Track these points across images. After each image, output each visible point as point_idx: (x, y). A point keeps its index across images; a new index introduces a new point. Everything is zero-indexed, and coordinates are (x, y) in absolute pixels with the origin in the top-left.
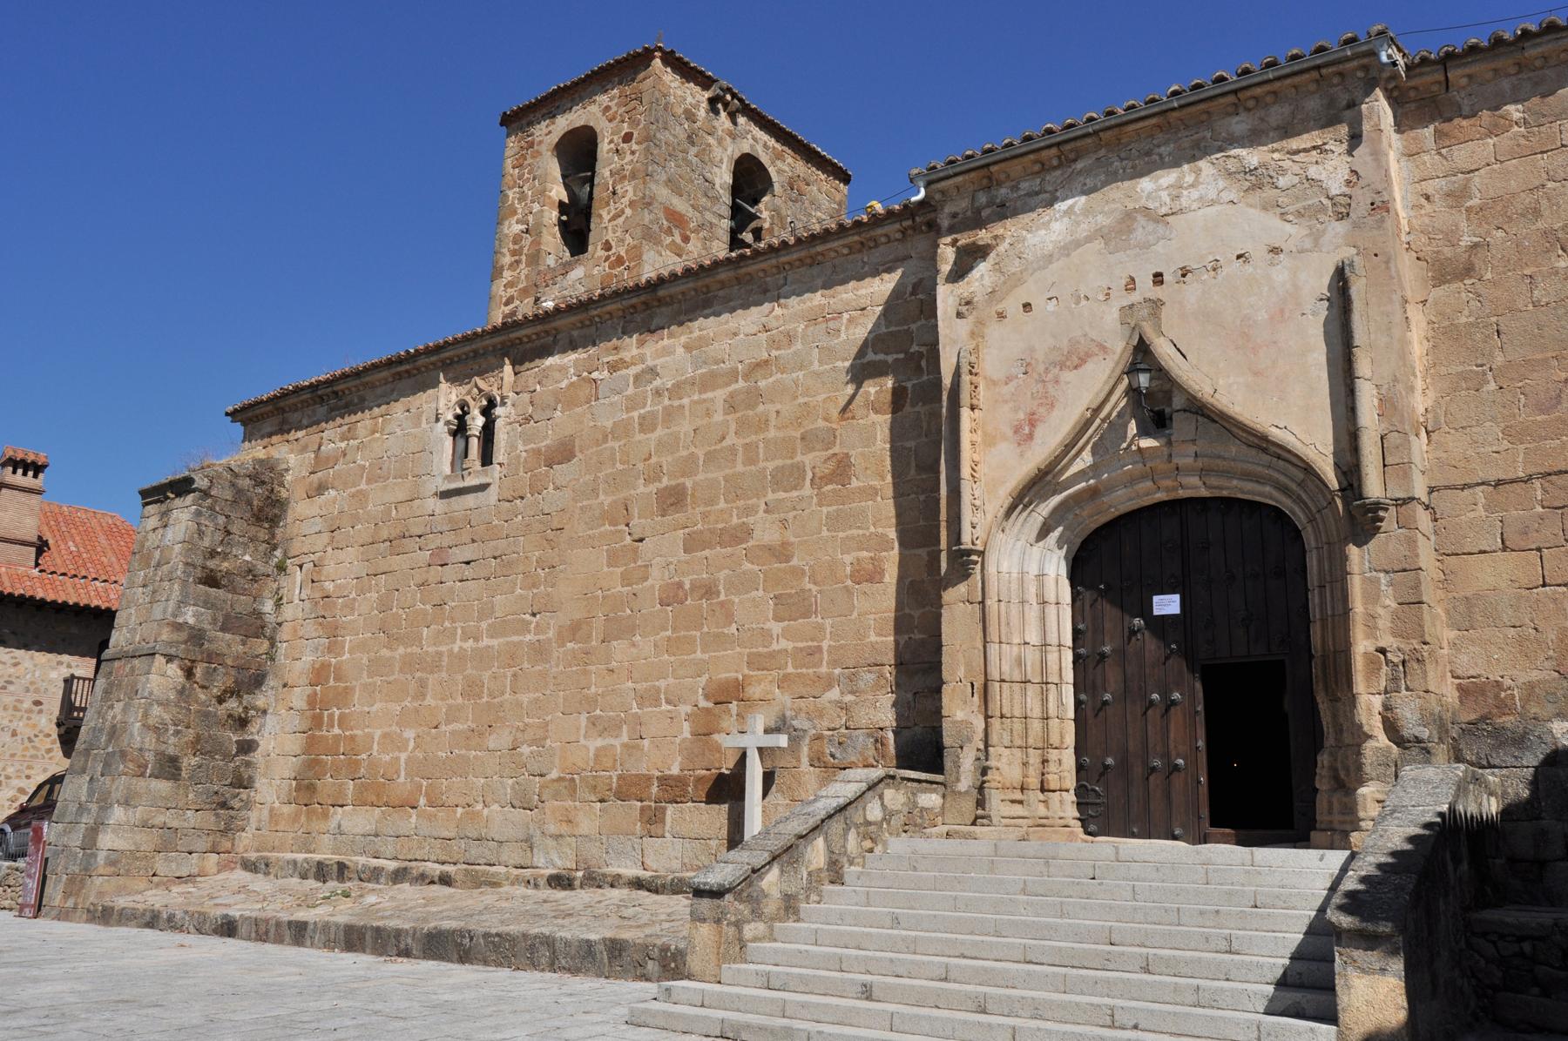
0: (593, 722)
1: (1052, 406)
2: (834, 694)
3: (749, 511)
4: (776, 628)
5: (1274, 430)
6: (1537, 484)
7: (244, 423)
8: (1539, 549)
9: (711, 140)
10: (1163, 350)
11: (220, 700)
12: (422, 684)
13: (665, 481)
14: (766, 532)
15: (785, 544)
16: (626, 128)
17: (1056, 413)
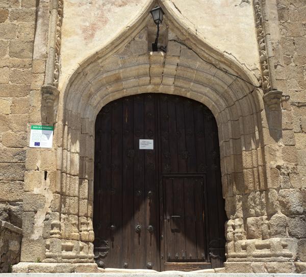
1: (106, 22)
5: (225, 53)
17: (107, 26)
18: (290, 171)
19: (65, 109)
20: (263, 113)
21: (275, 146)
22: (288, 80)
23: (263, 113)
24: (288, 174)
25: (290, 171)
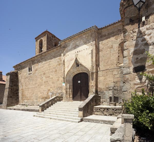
0: (40, 93)
2: (56, 90)
3: (50, 75)
4: (52, 85)
7: (15, 68)
9: (52, 40)
10: (78, 59)
11: (15, 92)
12: (29, 90)
13: (44, 72)
14: (51, 77)
15: (52, 77)
16: (45, 39)
19: (66, 80)
20: (91, 76)
21: (92, 82)
23: (91, 76)
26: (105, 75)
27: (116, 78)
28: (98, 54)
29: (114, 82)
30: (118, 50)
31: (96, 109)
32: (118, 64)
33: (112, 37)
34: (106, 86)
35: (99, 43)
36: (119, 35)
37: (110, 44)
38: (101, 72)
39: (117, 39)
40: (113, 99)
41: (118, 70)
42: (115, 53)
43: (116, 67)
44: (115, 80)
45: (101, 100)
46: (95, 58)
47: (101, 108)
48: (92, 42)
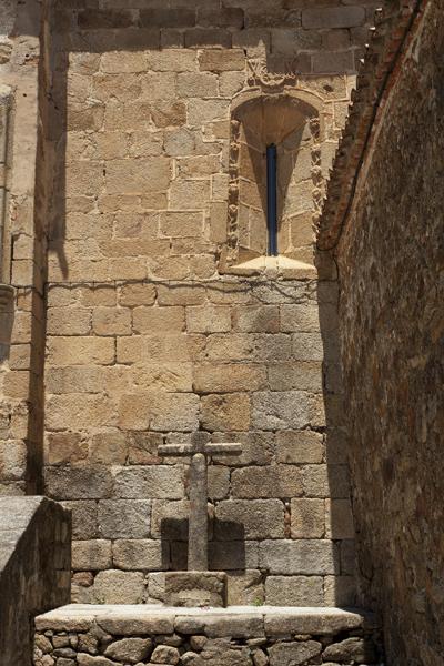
6: (119, 289)
8: (115, 336)
18: (12, 411)
22: (81, 242)
24: (10, 417)
25: (12, 411)
26: (122, 323)
27: (215, 363)
28: (49, 139)
29: (201, 394)
30: (226, 150)
31: (59, 640)
32: (232, 254)
33: (182, 50)
34: (127, 425)
35: (67, 64)
36: (236, 49)
37: (160, 91)
38: (80, 292)
39: (219, 73)
40: (198, 541)
41: (228, 298)
42: (203, 167)
43: (216, 276)
44: (211, 378)
45: (80, 551)
46: (33, 168)
47: (117, 629)
48: (12, 36)
